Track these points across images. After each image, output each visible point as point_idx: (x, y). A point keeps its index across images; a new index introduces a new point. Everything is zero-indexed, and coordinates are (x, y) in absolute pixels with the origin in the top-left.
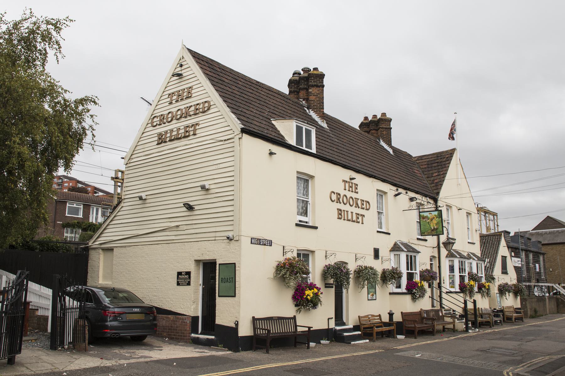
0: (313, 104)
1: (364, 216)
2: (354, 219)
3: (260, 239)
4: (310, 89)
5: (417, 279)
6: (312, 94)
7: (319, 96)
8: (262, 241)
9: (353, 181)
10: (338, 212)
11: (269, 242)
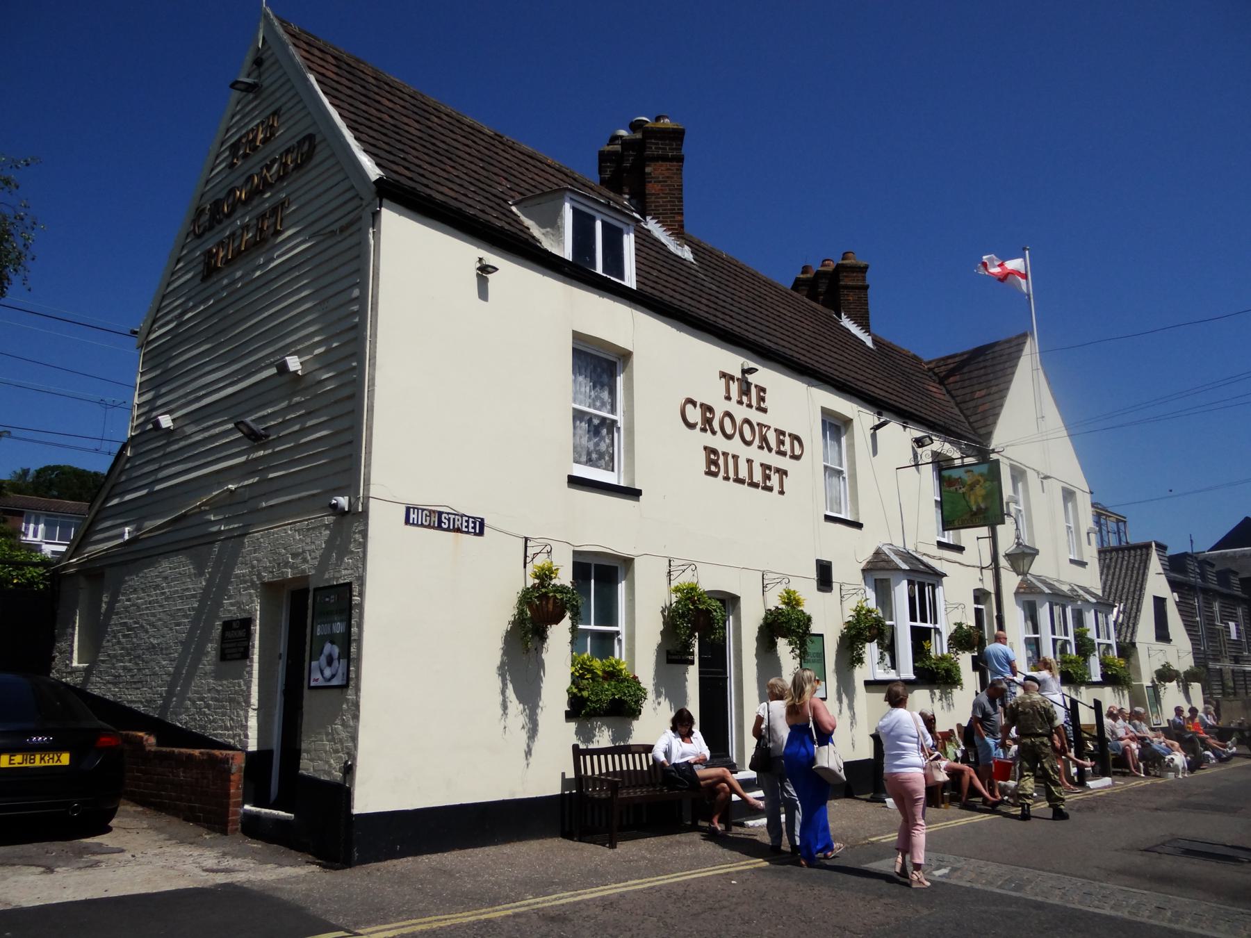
0: (655, 202)
1: (785, 473)
2: (758, 477)
3: (440, 513)
4: (649, 166)
5: (939, 647)
6: (652, 178)
7: (669, 183)
8: (449, 520)
9: (751, 378)
10: (708, 458)
11: (474, 523)
